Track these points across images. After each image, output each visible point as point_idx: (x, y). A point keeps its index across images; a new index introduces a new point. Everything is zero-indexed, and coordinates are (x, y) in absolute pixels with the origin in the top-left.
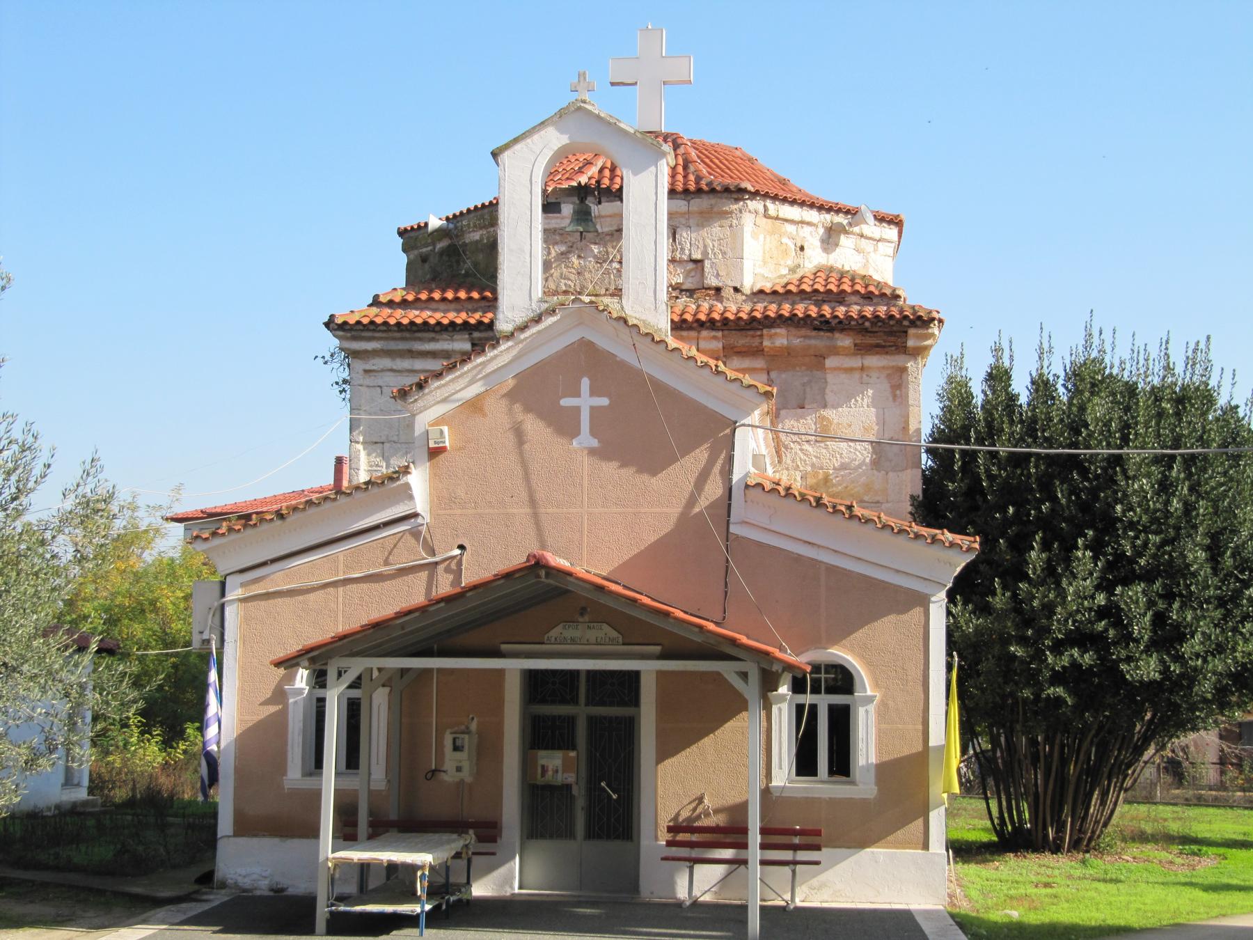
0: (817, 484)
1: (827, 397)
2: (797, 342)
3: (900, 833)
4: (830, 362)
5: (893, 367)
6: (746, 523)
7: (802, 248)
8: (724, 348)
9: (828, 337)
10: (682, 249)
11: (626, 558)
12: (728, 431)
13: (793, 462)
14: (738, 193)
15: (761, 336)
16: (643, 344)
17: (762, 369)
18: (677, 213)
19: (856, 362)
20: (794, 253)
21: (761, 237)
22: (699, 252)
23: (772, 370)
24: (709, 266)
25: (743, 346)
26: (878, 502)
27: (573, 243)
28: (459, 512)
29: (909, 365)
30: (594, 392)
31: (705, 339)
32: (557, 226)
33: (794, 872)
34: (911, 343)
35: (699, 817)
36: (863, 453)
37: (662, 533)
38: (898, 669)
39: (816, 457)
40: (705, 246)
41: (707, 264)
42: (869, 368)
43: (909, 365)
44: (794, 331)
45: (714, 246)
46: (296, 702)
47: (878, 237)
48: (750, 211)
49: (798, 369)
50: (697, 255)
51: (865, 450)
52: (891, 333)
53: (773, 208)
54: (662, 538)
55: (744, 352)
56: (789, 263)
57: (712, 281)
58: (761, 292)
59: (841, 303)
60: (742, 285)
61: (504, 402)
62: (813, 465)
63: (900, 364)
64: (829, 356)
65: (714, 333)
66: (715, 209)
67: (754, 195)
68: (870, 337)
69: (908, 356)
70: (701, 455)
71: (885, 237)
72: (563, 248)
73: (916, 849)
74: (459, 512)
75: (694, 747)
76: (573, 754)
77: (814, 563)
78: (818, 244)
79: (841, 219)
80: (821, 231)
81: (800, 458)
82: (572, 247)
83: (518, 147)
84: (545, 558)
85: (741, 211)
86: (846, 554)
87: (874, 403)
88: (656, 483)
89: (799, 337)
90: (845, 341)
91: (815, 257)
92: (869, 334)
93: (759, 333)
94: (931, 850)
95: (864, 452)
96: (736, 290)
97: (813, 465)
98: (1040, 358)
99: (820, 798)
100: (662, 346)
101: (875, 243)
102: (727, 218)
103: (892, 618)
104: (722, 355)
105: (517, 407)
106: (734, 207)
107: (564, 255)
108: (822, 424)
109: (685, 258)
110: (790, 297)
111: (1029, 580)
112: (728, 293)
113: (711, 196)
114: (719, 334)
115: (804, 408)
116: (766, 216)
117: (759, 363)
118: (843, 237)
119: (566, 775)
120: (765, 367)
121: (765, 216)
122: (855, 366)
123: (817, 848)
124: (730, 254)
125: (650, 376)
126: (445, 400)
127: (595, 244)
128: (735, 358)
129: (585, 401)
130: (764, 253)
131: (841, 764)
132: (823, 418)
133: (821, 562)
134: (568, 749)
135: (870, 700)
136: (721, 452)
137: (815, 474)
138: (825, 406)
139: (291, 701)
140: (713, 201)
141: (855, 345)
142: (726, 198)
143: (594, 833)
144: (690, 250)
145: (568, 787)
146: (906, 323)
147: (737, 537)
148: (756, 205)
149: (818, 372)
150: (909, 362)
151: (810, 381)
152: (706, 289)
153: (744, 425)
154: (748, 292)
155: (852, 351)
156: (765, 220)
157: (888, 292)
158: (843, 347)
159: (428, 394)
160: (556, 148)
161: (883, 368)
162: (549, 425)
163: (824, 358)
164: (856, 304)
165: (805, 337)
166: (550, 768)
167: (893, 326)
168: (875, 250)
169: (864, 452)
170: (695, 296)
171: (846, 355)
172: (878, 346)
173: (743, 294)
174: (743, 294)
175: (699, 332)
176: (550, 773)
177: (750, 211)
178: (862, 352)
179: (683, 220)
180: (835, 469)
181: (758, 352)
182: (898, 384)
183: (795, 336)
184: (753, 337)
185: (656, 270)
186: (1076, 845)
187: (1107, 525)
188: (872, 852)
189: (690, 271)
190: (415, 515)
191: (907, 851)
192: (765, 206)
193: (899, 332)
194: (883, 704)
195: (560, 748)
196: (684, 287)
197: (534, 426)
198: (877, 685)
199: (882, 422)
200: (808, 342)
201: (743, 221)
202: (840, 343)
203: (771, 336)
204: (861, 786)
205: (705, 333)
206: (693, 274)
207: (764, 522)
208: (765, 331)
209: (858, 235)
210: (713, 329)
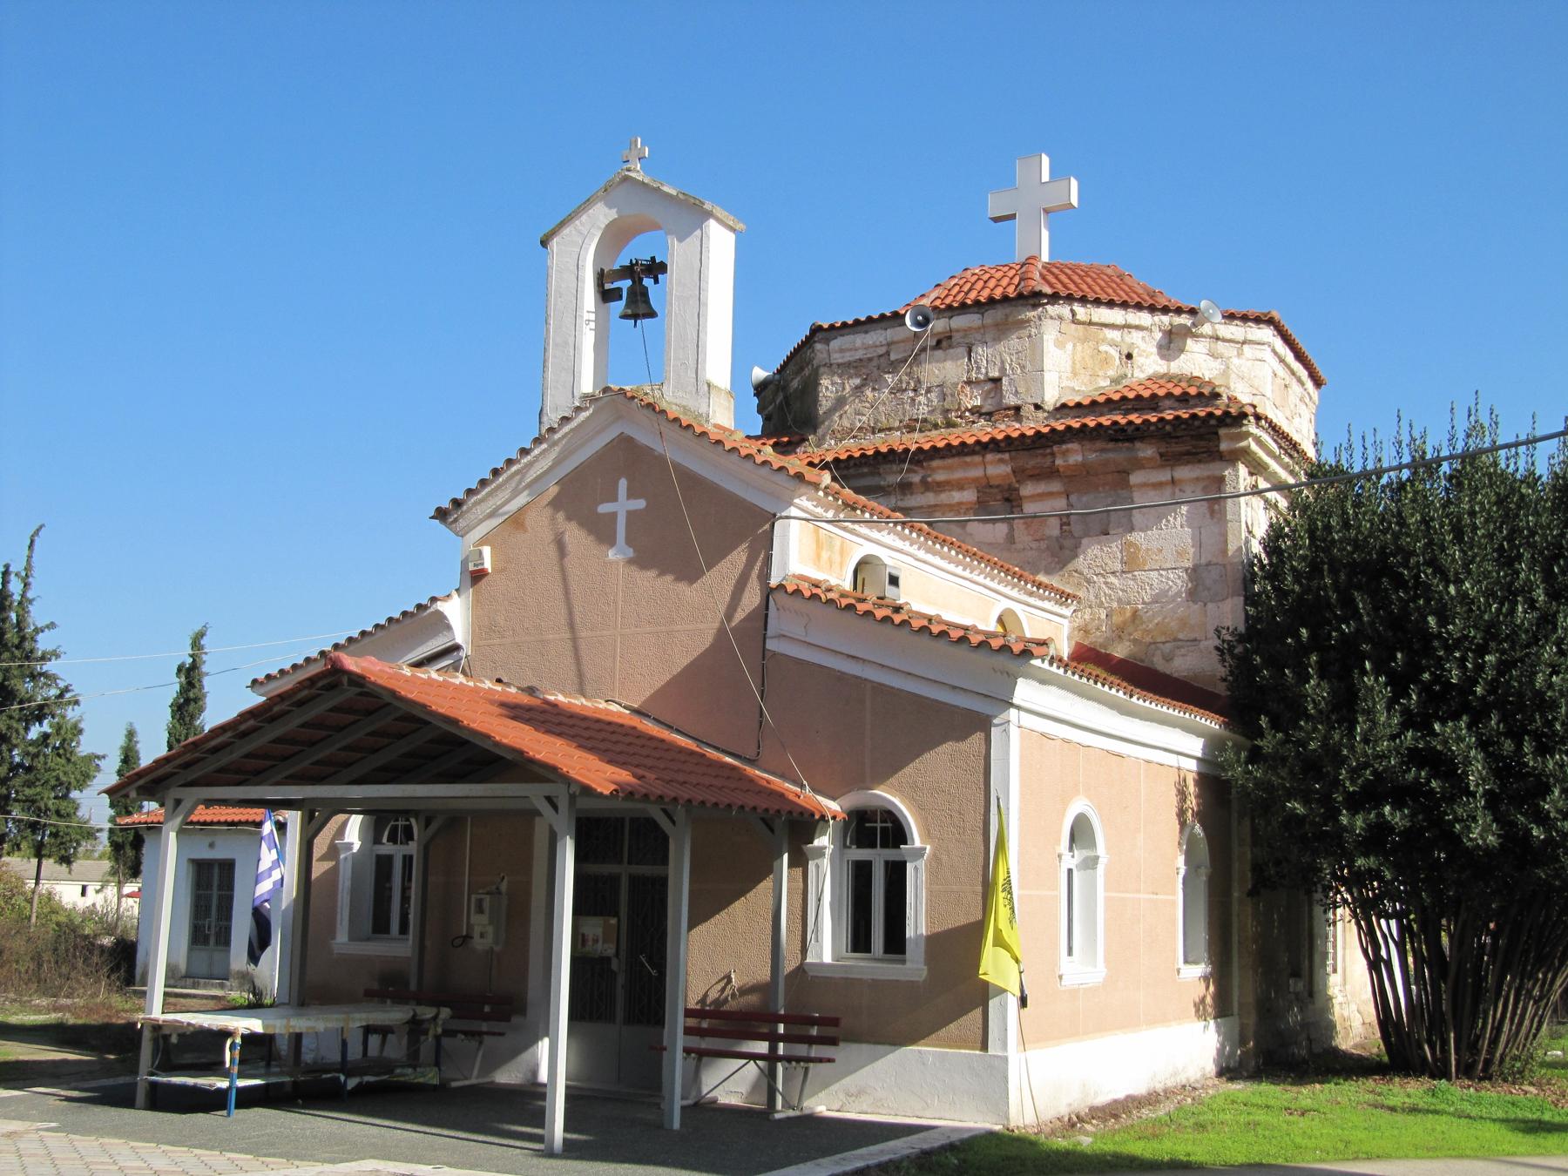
0: (1125, 623)
1: (1134, 520)
2: (1092, 456)
3: (943, 1032)
4: (1136, 478)
5: (1209, 477)
6: (784, 636)
7: (1129, 356)
8: (1014, 472)
9: (1128, 449)
10: (979, 368)
11: (658, 685)
12: (767, 527)
13: (1096, 597)
14: (1033, 299)
15: (1053, 454)
16: (671, 432)
17: (1062, 493)
18: (970, 328)
19: (1164, 475)
20: (1118, 362)
21: (1069, 346)
22: (997, 369)
23: (1073, 493)
25: (1034, 467)
26: (1195, 640)
27: (867, 375)
28: (497, 641)
29: (1226, 473)
30: (631, 495)
31: (991, 463)
32: (851, 359)
33: (807, 1069)
34: (1224, 446)
35: (726, 1000)
36: (1177, 582)
37: (696, 654)
38: (953, 814)
39: (1122, 590)
40: (1003, 362)
41: (1005, 381)
42: (1181, 481)
43: (1226, 473)
44: (1088, 445)
45: (1012, 360)
46: (346, 858)
47: (1241, 339)
48: (1051, 318)
49: (1101, 489)
50: (995, 374)
52: (1200, 437)
54: (695, 660)
55: (1038, 475)
56: (1111, 373)
57: (1011, 400)
58: (1064, 406)
59: (1155, 409)
60: (1043, 401)
61: (549, 511)
62: (1119, 600)
63: (1217, 473)
65: (999, 456)
66: (1010, 320)
67: (1055, 298)
68: (1176, 443)
69: (1225, 463)
70: (739, 556)
71: (1250, 337)
72: (857, 381)
73: (973, 1049)
74: (497, 641)
75: (723, 913)
76: (613, 921)
77: (859, 681)
78: (1155, 350)
79: (1185, 320)
80: (1159, 335)
82: (866, 379)
83: (566, 231)
84: (341, 661)
85: (1040, 319)
87: (1190, 521)
88: (689, 593)
89: (1096, 451)
90: (1147, 451)
91: (1149, 365)
92: (1174, 440)
93: (1048, 451)
94: (991, 1051)
95: (1178, 581)
96: (1037, 407)
97: (1119, 600)
98: (1398, 453)
99: (860, 980)
100: (690, 432)
101: (1239, 346)
102: (1026, 328)
103: (947, 747)
104: (1014, 480)
105: (561, 516)
106: (1031, 314)
107: (858, 389)
108: (1129, 551)
109: (982, 377)
110: (1097, 409)
111: (1308, 717)
112: (1028, 410)
113: (1006, 305)
114: (1006, 456)
116: (1075, 321)
117: (1056, 486)
118: (1189, 342)
119: (606, 946)
120: (1063, 490)
121: (1073, 322)
122: (1163, 479)
123: (833, 1042)
125: (677, 466)
126: (492, 515)
127: (889, 373)
129: (623, 505)
130: (1074, 363)
131: (896, 942)
132: (1131, 544)
133: (866, 680)
134: (609, 915)
135: (920, 853)
136: (760, 553)
137: (1122, 611)
138: (1132, 529)
139: (342, 856)
140: (1008, 311)
141: (1161, 455)
142: (1022, 305)
143: (630, 1019)
144: (987, 368)
145: (606, 960)
146: (1213, 422)
147: (774, 654)
148: (1063, 310)
152: (1005, 409)
153: (781, 518)
154: (1051, 408)
155: (1159, 462)
156: (1073, 326)
157: (1206, 391)
158: (1145, 458)
159: (467, 512)
160: (603, 226)
161: (1197, 479)
162: (590, 532)
163: (1128, 474)
164: (1171, 408)
165: (1103, 450)
166: (590, 937)
167: (1199, 427)
168: (1239, 355)
169: (1178, 581)
170: (993, 419)
171: (1153, 468)
172: (1188, 453)
173: (1045, 411)
174: (1045, 411)
175: (983, 456)
176: (590, 943)
177: (1051, 318)
178: (1171, 463)
179: (978, 337)
181: (1051, 473)
182: (1216, 501)
183: (1090, 450)
184: (1045, 456)
185: (698, 346)
186: (1467, 1071)
187: (1422, 646)
188: (920, 1052)
189: (989, 392)
190: (457, 648)
191: (963, 1051)
192: (1072, 311)
193: (1208, 434)
194: (935, 857)
195: (601, 914)
196: (984, 411)
197: (575, 536)
198: (927, 834)
199: (1199, 545)
200: (1105, 456)
201: (1043, 329)
202: (1141, 454)
203: (1064, 453)
204: (908, 965)
205: (989, 457)
206: (992, 395)
207: (798, 632)
208: (1055, 448)
209: (1211, 337)
210: (999, 452)
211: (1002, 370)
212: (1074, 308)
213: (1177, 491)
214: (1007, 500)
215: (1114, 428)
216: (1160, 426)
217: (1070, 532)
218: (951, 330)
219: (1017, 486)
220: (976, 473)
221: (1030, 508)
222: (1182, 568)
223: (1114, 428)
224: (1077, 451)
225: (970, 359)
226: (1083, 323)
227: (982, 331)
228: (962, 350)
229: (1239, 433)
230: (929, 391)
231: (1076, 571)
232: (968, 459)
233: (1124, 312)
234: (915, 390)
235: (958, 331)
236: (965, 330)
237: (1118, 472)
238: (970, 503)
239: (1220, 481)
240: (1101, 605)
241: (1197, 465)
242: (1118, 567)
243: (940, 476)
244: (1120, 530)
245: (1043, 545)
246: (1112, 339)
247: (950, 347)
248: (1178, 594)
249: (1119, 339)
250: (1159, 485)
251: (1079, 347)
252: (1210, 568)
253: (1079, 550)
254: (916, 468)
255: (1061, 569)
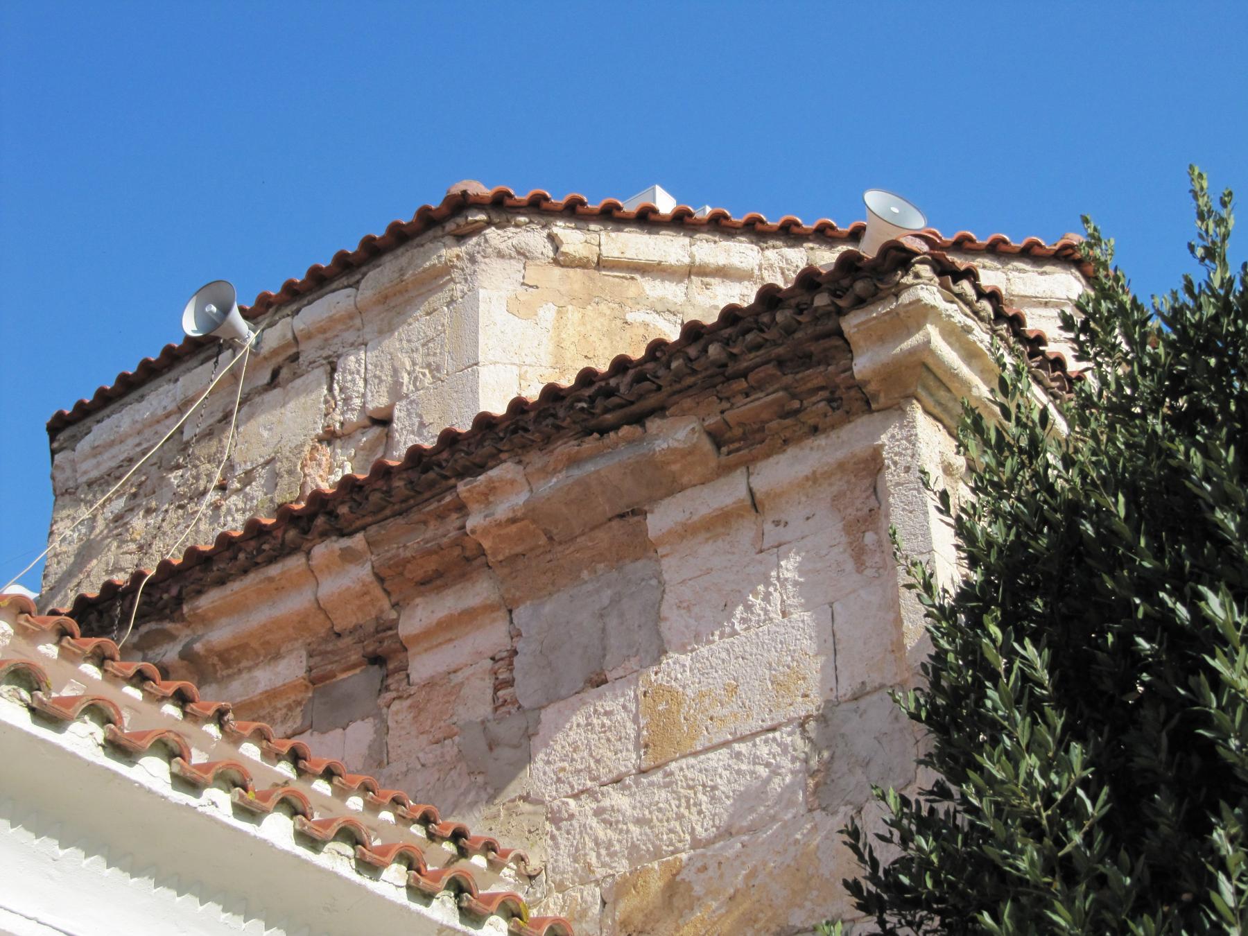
4: (659, 521)
5: (841, 466)
8: (380, 579)
9: (631, 442)
17: (489, 608)
19: (731, 491)
21: (548, 313)
24: (403, 414)
29: (884, 438)
34: (863, 364)
39: (639, 822)
40: (395, 372)
42: (774, 496)
44: (536, 459)
45: (414, 364)
48: (500, 255)
49: (585, 574)
51: (785, 751)
52: (806, 360)
53: (573, 238)
55: (439, 574)
62: (633, 852)
64: (654, 500)
81: (597, 842)
82: (135, 495)
85: (472, 260)
86: (54, 928)
97: (633, 852)
104: (386, 604)
106: (449, 252)
114: (358, 541)
115: (605, 682)
116: (561, 260)
117: (480, 592)
121: (556, 262)
124: (448, 365)
128: (418, 600)
130: (559, 346)
146: (821, 300)
148: (532, 237)
149: (639, 564)
150: (884, 430)
151: (616, 600)
156: (558, 271)
158: (673, 451)
161: (814, 479)
165: (574, 461)
180: (696, 843)
184: (441, 516)
192: (552, 238)
199: (833, 646)
201: (482, 279)
205: (322, 550)
208: (462, 488)
211: (396, 393)
212: (555, 230)
213: (768, 527)
214: (377, 660)
215: (587, 392)
216: (692, 351)
217: (515, 701)
218: (295, 338)
219: (393, 615)
220: (296, 603)
221: (423, 666)
222: (790, 721)
223: (587, 392)
224: (513, 482)
225: (330, 389)
226: (582, 264)
227: (358, 322)
228: (320, 373)
229: (894, 314)
230: (248, 478)
231: (525, 798)
232: (274, 570)
233: (687, 240)
234: (222, 487)
235: (309, 336)
236: (323, 330)
237: (622, 516)
238: (293, 687)
239: (873, 465)
240: (587, 873)
241: (809, 442)
242: (629, 760)
243: (221, 635)
244: (633, 663)
245: (450, 749)
246: (661, 300)
247: (296, 375)
248: (785, 799)
249: (681, 298)
250: (721, 521)
251: (573, 314)
252: (863, 703)
253: (536, 741)
254: (168, 625)
255: (491, 799)
